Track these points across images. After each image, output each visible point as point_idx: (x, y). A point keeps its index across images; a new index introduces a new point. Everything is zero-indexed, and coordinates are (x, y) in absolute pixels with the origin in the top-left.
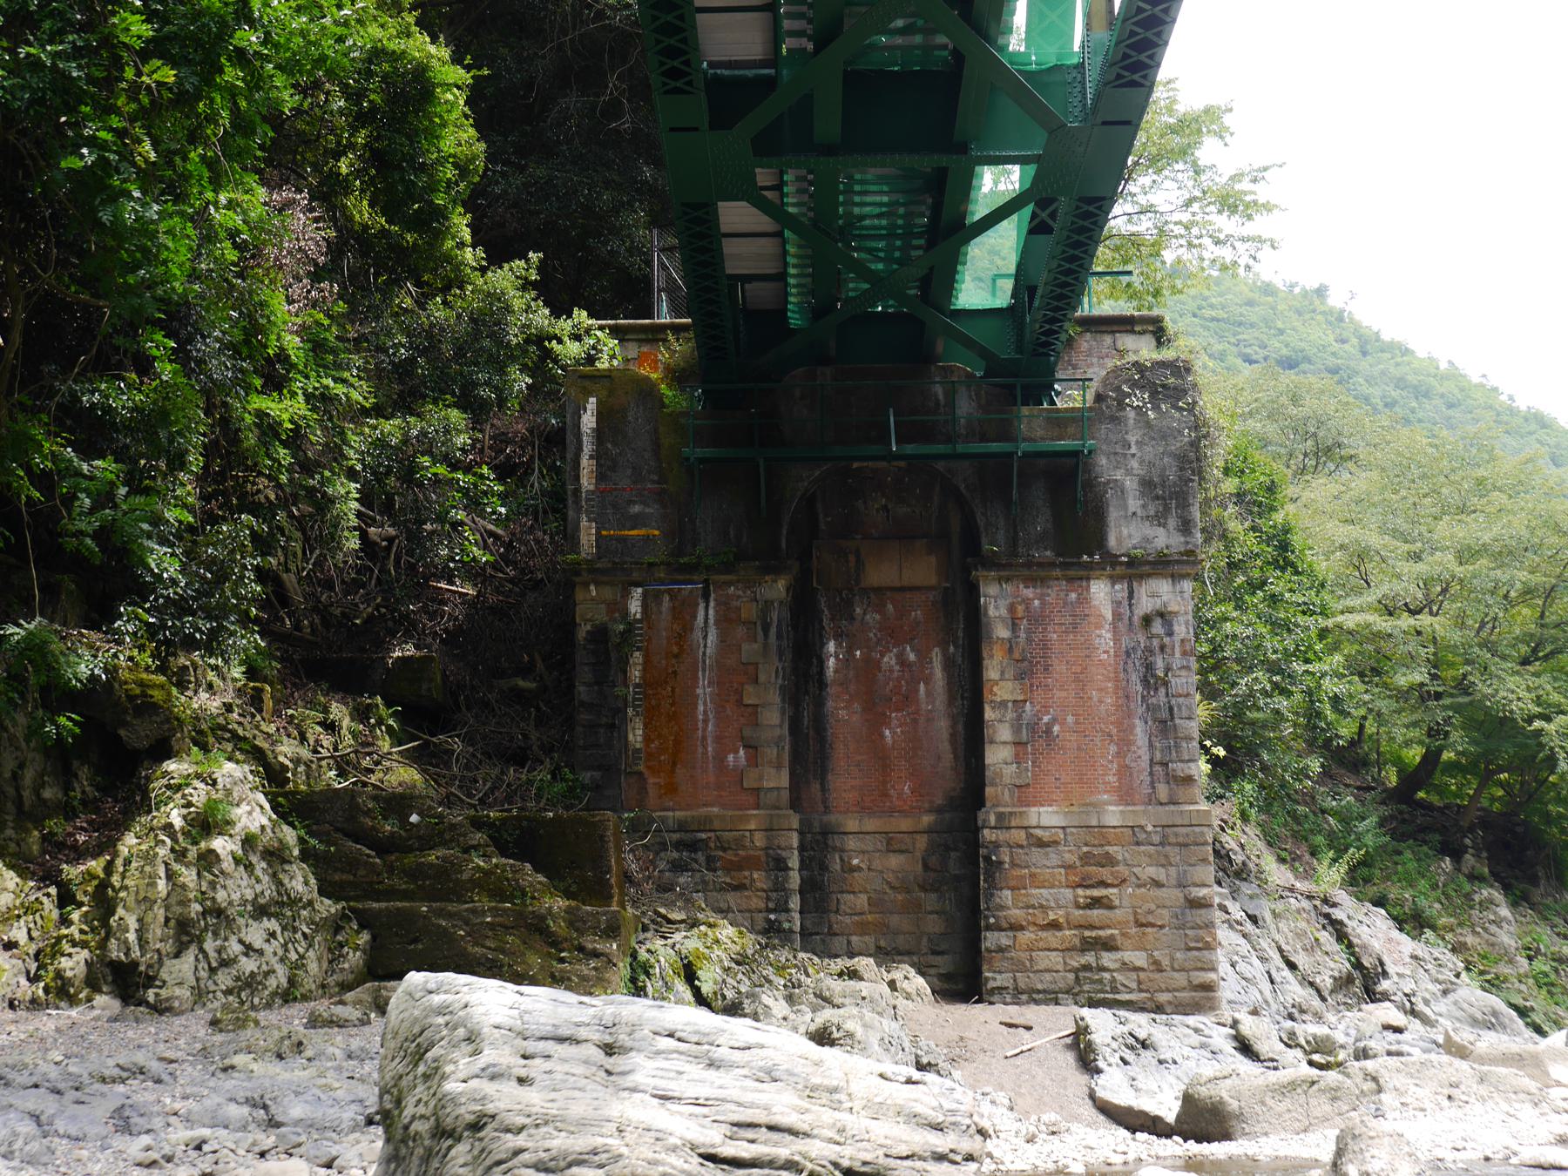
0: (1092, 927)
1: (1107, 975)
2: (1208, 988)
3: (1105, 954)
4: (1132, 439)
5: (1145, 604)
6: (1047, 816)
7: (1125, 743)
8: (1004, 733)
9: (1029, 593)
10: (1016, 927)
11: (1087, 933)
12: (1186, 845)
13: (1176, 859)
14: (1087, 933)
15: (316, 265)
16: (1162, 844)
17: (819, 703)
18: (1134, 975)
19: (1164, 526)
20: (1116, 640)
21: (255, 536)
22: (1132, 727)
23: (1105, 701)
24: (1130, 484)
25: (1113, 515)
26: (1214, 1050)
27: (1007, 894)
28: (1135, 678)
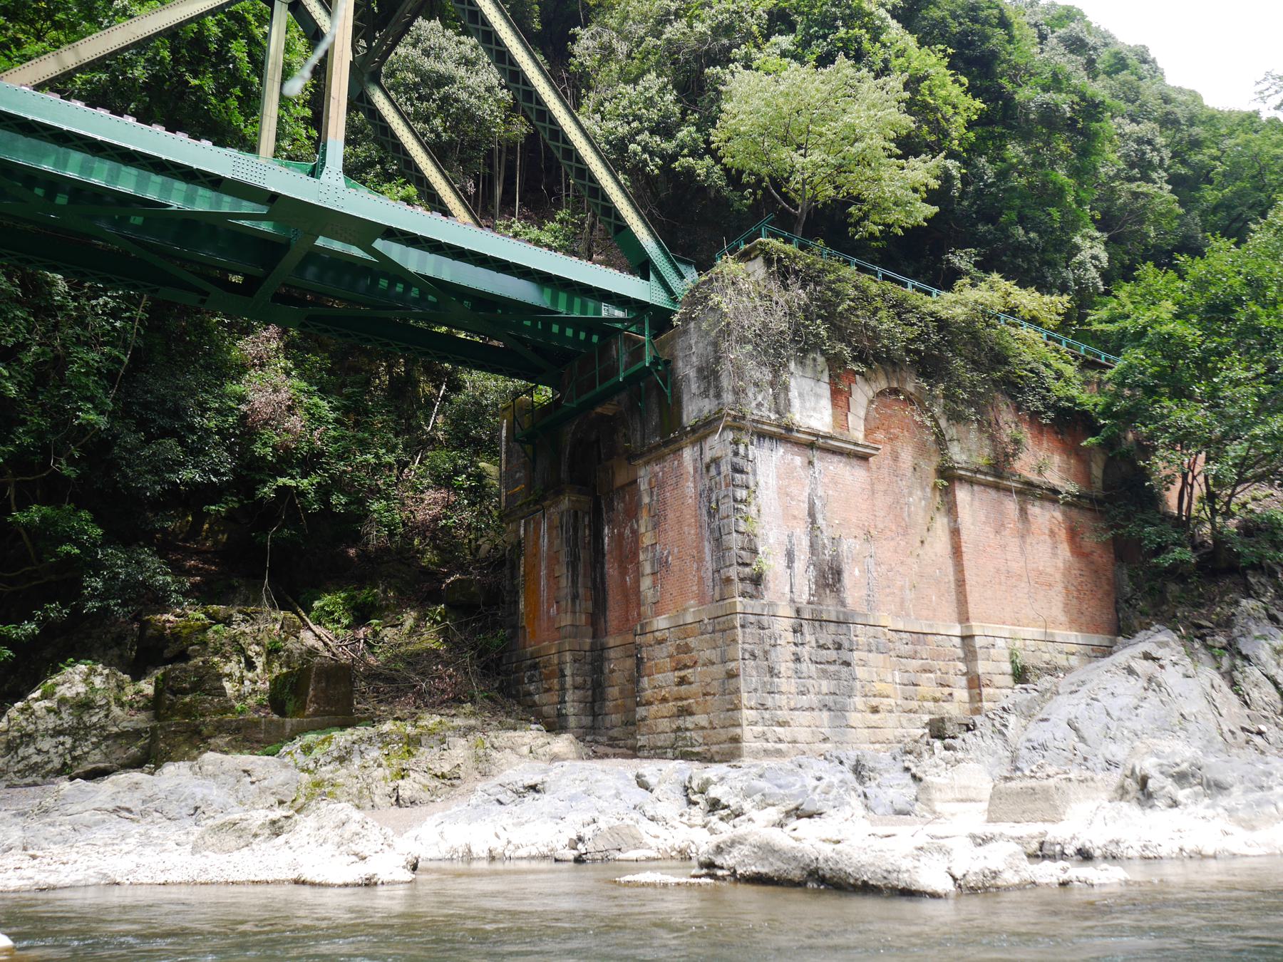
0: (681, 699)
1: (688, 734)
2: (736, 740)
3: (688, 718)
4: (693, 342)
5: (708, 456)
6: (661, 623)
7: (701, 560)
8: (647, 569)
9: (657, 468)
10: (649, 703)
11: (680, 704)
12: (724, 631)
13: (720, 642)
14: (680, 704)
15: (851, 225)
16: (713, 632)
17: (603, 567)
18: (701, 732)
19: (707, 396)
20: (695, 487)
21: (716, 461)
22: (703, 547)
23: (690, 532)
24: (692, 374)
25: (685, 398)
26: (862, 798)
27: (646, 679)
28: (704, 512)
